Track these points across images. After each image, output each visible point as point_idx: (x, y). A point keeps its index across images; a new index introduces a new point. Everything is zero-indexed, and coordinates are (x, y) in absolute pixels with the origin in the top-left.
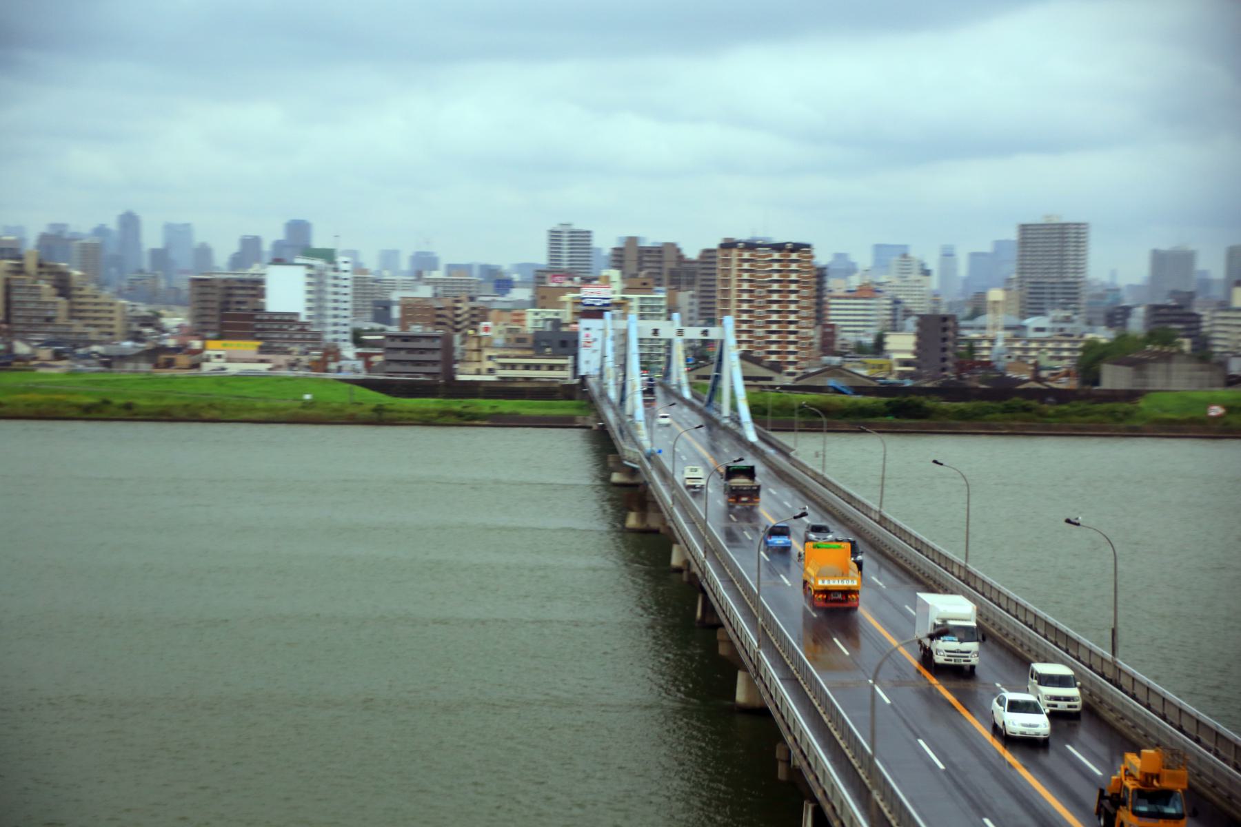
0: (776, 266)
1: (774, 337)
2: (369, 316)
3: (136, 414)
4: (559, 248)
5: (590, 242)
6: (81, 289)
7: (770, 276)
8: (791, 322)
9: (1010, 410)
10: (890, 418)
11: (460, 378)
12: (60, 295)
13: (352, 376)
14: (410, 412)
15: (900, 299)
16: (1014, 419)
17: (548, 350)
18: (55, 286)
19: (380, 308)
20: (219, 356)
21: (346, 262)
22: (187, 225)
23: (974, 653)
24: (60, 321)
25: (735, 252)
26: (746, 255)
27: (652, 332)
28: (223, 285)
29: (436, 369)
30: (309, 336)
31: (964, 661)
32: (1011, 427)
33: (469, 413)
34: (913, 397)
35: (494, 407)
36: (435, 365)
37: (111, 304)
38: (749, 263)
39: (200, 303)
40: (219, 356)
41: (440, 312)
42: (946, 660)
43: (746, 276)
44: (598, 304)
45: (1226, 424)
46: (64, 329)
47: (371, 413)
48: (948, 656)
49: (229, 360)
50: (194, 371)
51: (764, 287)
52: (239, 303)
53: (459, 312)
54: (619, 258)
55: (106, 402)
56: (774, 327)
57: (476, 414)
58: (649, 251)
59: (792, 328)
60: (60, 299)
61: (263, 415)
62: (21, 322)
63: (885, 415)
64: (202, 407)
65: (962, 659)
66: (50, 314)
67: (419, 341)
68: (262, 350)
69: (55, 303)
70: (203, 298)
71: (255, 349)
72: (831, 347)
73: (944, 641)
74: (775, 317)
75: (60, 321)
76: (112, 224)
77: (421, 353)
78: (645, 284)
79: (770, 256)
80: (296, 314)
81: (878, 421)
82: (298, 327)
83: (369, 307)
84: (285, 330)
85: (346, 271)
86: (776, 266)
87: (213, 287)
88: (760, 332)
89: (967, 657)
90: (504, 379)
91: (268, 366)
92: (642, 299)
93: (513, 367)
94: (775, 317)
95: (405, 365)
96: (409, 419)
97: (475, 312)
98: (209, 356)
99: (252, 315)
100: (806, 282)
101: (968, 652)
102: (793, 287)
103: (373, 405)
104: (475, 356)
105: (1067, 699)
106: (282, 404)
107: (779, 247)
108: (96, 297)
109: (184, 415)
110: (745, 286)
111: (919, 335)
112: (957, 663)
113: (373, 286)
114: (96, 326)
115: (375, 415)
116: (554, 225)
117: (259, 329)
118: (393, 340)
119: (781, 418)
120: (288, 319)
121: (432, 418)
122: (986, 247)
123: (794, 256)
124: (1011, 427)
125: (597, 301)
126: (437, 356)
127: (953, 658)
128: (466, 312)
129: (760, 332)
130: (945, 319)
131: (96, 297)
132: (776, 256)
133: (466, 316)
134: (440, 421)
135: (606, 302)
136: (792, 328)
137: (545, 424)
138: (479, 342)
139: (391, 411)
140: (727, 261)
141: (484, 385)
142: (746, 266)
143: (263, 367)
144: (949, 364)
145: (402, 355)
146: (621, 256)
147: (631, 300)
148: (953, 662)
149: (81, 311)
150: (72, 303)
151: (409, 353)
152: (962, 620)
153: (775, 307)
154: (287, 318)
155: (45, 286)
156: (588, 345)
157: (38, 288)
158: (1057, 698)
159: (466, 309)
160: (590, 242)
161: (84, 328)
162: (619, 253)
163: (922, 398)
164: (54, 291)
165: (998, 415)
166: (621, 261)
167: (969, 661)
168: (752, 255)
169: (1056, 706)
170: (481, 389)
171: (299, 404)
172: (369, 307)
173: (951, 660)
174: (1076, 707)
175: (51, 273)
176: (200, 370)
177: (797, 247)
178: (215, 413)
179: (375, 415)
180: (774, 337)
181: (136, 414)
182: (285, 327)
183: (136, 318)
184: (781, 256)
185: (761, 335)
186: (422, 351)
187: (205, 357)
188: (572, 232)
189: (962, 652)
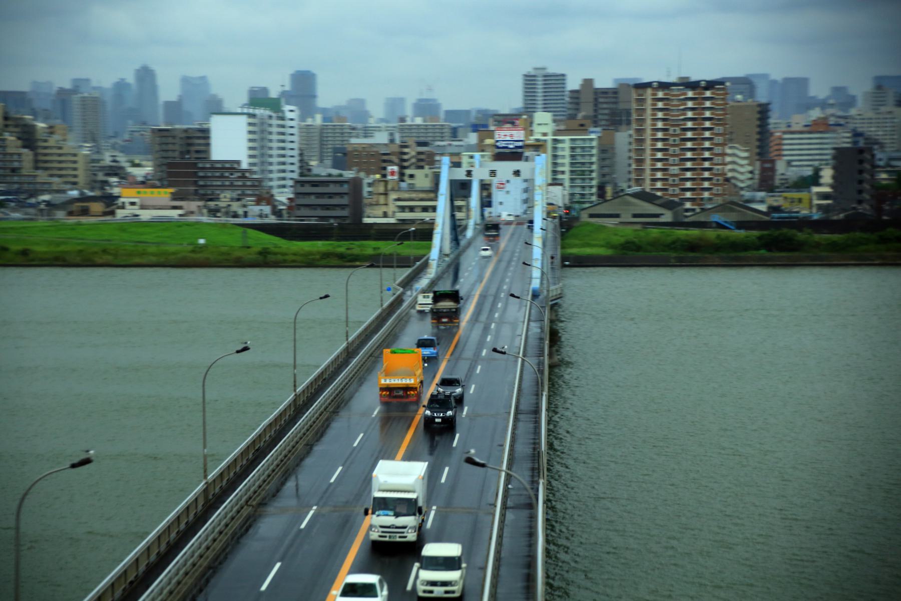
0: (690, 104)
1: (689, 175)
2: (328, 162)
3: (33, 260)
4: (534, 92)
5: (564, 82)
6: (46, 141)
7: (685, 114)
8: (705, 159)
11: (367, 220)
12: (24, 147)
13: (258, 221)
14: (295, 254)
15: (870, 135)
18: (19, 138)
19: (339, 154)
20: (133, 204)
21: (291, 111)
22: (203, 78)
23: (411, 528)
24: (24, 172)
25: (649, 91)
26: (660, 94)
27: (465, 173)
28: (184, 135)
29: (345, 213)
30: (249, 183)
31: (400, 537)
33: (352, 255)
34: (785, 230)
35: (375, 249)
36: (343, 209)
37: (75, 155)
38: (693, 102)
39: (161, 153)
40: (133, 204)
41: (385, 158)
42: (380, 536)
43: (660, 115)
44: (511, 146)
46: (30, 180)
47: (258, 256)
48: (383, 532)
49: (143, 207)
50: (108, 218)
51: (678, 125)
52: (197, 152)
53: (406, 157)
54: (576, 101)
56: (689, 165)
57: (357, 256)
58: (604, 92)
59: (707, 164)
60: (25, 151)
61: (154, 259)
64: (96, 253)
65: (398, 535)
66: (16, 165)
67: (328, 186)
68: (175, 197)
69: (19, 155)
70: (164, 147)
71: (169, 196)
72: (770, 182)
73: (378, 516)
74: (689, 155)
75: (24, 172)
77: (330, 197)
78: (582, 125)
79: (685, 94)
80: (238, 162)
81: (749, 255)
82: (239, 174)
83: (329, 154)
84: (227, 177)
85: (292, 119)
86: (690, 104)
87: (174, 137)
88: (675, 170)
89: (403, 533)
90: (403, 221)
92: (572, 140)
93: (412, 209)
94: (689, 155)
95: (315, 209)
96: (294, 261)
97: (422, 157)
98: (123, 203)
99: (196, 164)
100: (719, 120)
101: (404, 527)
102: (707, 124)
103: (258, 248)
104: (382, 199)
105: (444, 584)
106: (172, 249)
108: (60, 148)
109: (78, 260)
110: (660, 125)
111: (834, 168)
112: (392, 540)
113: (351, 133)
114: (60, 176)
115: (261, 258)
116: (529, 70)
118: (302, 186)
119: (654, 254)
120: (231, 167)
121: (314, 259)
123: (708, 94)
125: (510, 144)
126: (345, 201)
127: (388, 535)
128: (413, 157)
129: (675, 170)
131: (60, 148)
132: (690, 94)
133: (414, 160)
134: (323, 262)
135: (520, 144)
136: (707, 164)
137: (664, 264)
138: (386, 186)
139: (275, 254)
140: (641, 101)
141: (375, 227)
142: (660, 105)
143: (175, 213)
144: (866, 196)
145: (312, 200)
146: (577, 98)
148: (387, 539)
149: (46, 162)
150: (36, 155)
151: (317, 197)
152: (405, 491)
153: (689, 145)
154: (227, 165)
156: (502, 186)
158: (434, 583)
159: (413, 153)
160: (564, 82)
162: (575, 95)
163: (794, 231)
164: (19, 143)
166: (578, 104)
167: (405, 537)
168: (665, 94)
169: (431, 592)
170: (373, 232)
171: (190, 248)
172: (329, 154)
173: (385, 537)
174: (453, 592)
175: (16, 126)
176: (114, 217)
178: (108, 258)
179: (261, 258)
180: (689, 175)
181: (33, 260)
182: (227, 174)
183: (102, 168)
184: (695, 94)
185: (676, 172)
186: (331, 195)
187: (120, 204)
188: (545, 76)
189: (397, 528)
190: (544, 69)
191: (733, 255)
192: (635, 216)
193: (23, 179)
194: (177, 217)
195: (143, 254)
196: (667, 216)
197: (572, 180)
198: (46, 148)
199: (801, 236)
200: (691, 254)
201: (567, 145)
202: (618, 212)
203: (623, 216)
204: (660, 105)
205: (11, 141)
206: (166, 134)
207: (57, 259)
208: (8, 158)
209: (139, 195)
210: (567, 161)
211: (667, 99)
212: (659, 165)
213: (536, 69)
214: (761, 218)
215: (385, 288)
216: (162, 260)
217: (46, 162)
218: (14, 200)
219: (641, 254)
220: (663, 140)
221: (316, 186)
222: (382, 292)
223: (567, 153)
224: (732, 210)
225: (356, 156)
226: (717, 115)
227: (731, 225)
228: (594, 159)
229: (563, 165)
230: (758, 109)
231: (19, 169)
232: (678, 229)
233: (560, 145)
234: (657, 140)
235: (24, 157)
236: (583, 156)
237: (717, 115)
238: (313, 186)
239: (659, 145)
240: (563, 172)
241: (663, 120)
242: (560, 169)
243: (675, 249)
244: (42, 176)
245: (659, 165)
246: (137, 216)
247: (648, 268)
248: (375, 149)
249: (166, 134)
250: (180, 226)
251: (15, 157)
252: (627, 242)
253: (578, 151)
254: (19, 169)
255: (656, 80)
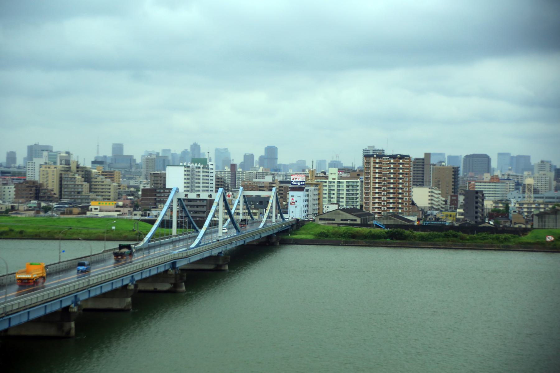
1: (391, 201)
3: (24, 236)
6: (96, 178)
9: (447, 236)
10: (388, 240)
12: (85, 181)
16: (449, 241)
17: (500, 216)
18: (83, 177)
20: (96, 209)
24: (83, 193)
25: (372, 159)
26: (377, 161)
32: (446, 245)
34: (399, 229)
37: (110, 185)
40: (96, 209)
43: (377, 171)
45: (555, 245)
49: (101, 211)
55: (11, 230)
56: (391, 196)
59: (400, 196)
60: (86, 183)
62: (66, 194)
63: (386, 238)
64: (56, 233)
66: (80, 190)
67: (196, 201)
69: (82, 185)
71: (114, 205)
74: (392, 191)
76: (259, 152)
77: (197, 207)
86: (392, 166)
88: (385, 198)
91: (118, 213)
92: (347, 182)
99: (156, 190)
100: (407, 174)
102: (401, 176)
107: (394, 157)
108: (103, 182)
109: (46, 236)
110: (377, 176)
114: (102, 196)
117: (159, 197)
119: (334, 239)
122: (192, 144)
123: (401, 161)
124: (446, 245)
129: (385, 198)
130: (477, 192)
131: (103, 182)
132: (392, 161)
135: (304, 183)
136: (400, 196)
142: (377, 166)
143: (115, 214)
147: (343, 183)
150: (91, 185)
151: (190, 207)
153: (392, 186)
155: (78, 177)
157: (75, 178)
161: (96, 197)
163: (404, 230)
164: (83, 179)
165: (441, 239)
177: (402, 157)
178: (61, 235)
181: (24, 236)
186: (198, 206)
188: (373, 151)
190: (374, 147)
191: (372, 241)
192: (342, 220)
193: (83, 197)
194: (116, 216)
195: (80, 234)
196: (359, 221)
197: (347, 202)
198: (96, 182)
199: (407, 232)
200: (352, 240)
201: (345, 184)
202: (334, 218)
203: (336, 220)
204: (377, 166)
205: (79, 178)
206: (157, 175)
207: (36, 235)
208: (76, 187)
209: (99, 205)
210: (345, 192)
211: (381, 163)
212: (377, 195)
213: (369, 147)
214: (405, 223)
215: (61, 251)
216: (88, 237)
217: (96, 189)
218: (63, 207)
219: (328, 238)
220: (379, 183)
221: (191, 201)
222: (60, 253)
223: (345, 188)
224: (391, 219)
225: (246, 188)
226: (405, 172)
227: (382, 225)
228: (358, 192)
229: (343, 194)
230: (453, 170)
231: (82, 192)
232: (355, 227)
233: (341, 184)
234: (376, 183)
235: (84, 186)
236: (353, 190)
237: (405, 172)
238: (189, 201)
239: (377, 186)
240: (343, 198)
241: (379, 173)
242: (341, 196)
243: (345, 237)
244: (92, 195)
245: (377, 195)
246: (97, 215)
247: (386, 248)
248: (256, 184)
249: (157, 175)
250: (108, 220)
251: (80, 186)
252: (322, 233)
253: (350, 188)
254: (82, 192)
255: (400, 154)
